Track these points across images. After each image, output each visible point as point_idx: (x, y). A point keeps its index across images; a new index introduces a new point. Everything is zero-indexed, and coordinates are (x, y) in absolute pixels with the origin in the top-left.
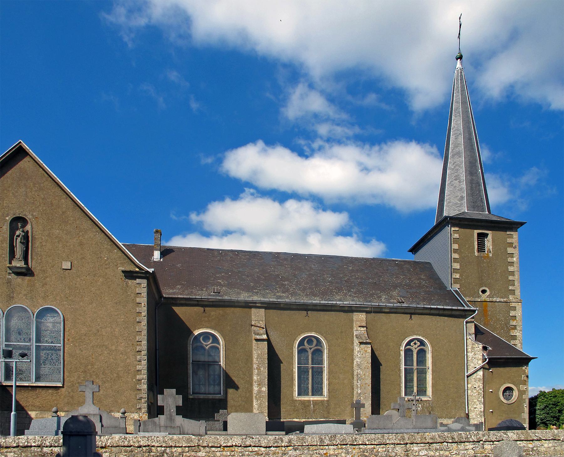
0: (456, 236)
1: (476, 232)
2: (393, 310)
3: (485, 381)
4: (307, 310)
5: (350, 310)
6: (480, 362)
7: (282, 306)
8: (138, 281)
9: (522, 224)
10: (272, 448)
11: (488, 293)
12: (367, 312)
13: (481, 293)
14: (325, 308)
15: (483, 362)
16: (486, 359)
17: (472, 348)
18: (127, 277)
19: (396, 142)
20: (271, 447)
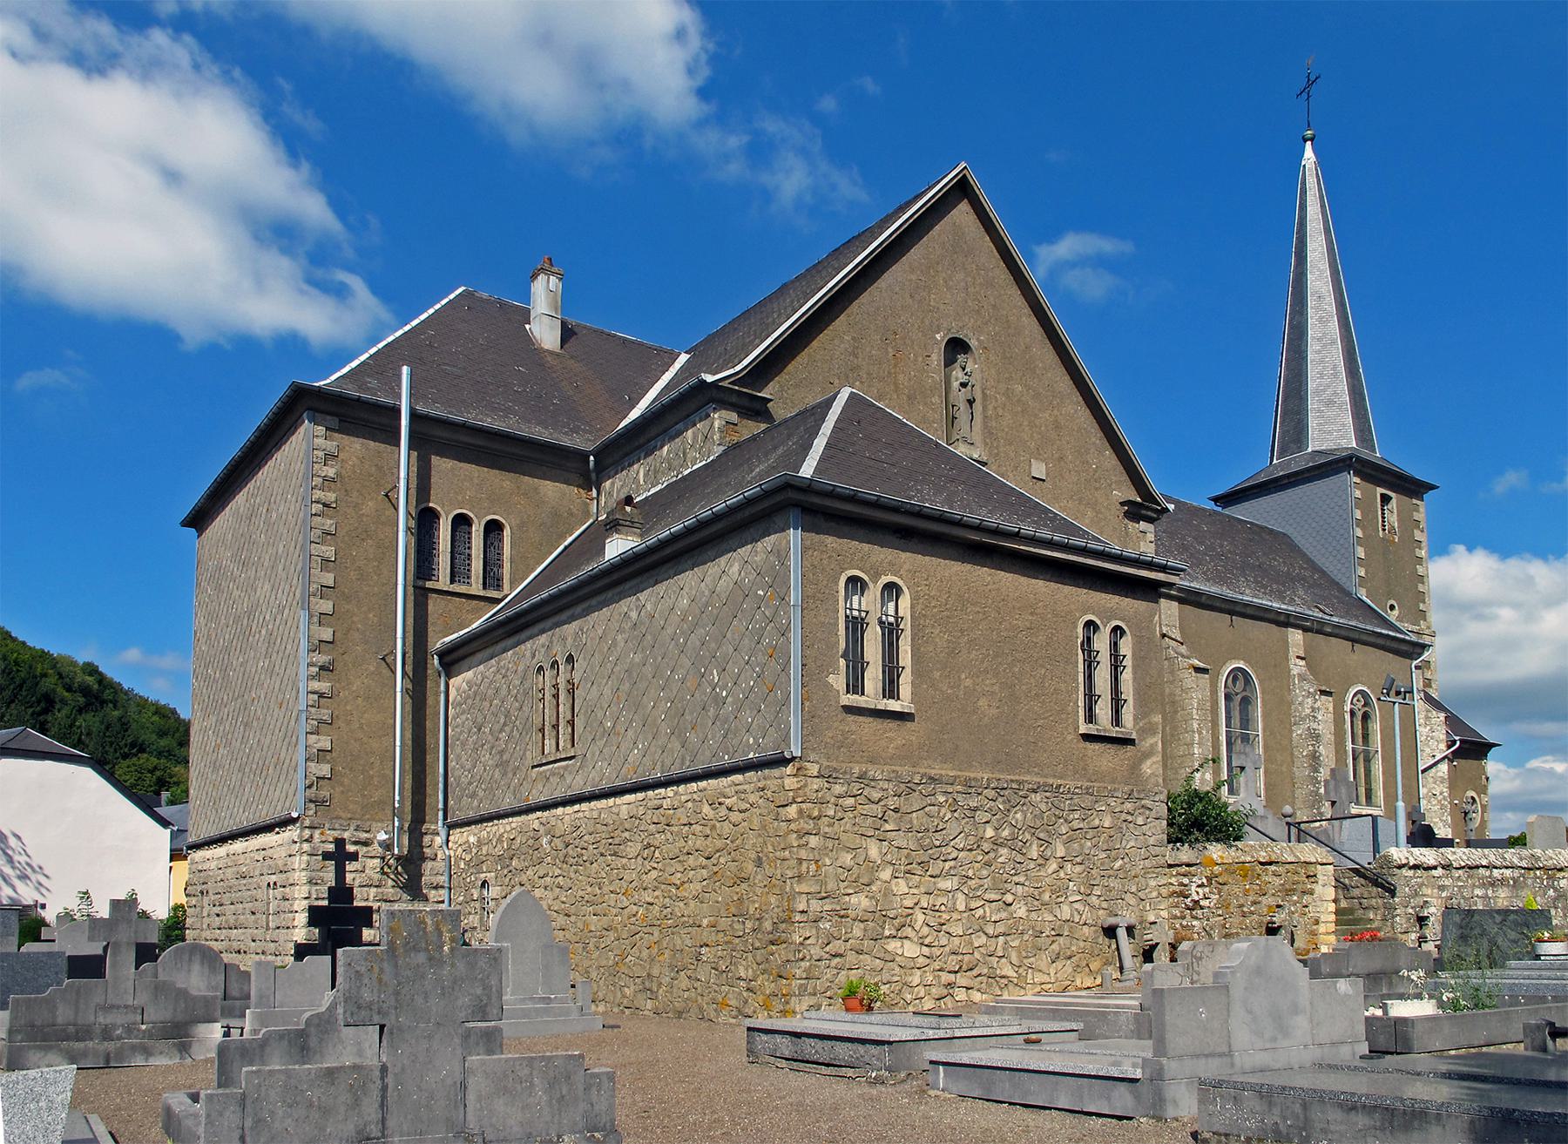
0: (1358, 494)
1: (1380, 490)
2: (1337, 631)
3: (1454, 782)
4: (1231, 613)
5: (1285, 621)
6: (1443, 746)
7: (1204, 599)
8: (1143, 525)
9: (1433, 487)
10: (1404, 870)
11: (1396, 612)
12: (1305, 630)
13: (885, 579)
14: (1262, 614)
15: (1449, 747)
16: (1454, 742)
17: (1427, 718)
18: (1127, 515)
19: (227, 78)
20: (1477, 867)
